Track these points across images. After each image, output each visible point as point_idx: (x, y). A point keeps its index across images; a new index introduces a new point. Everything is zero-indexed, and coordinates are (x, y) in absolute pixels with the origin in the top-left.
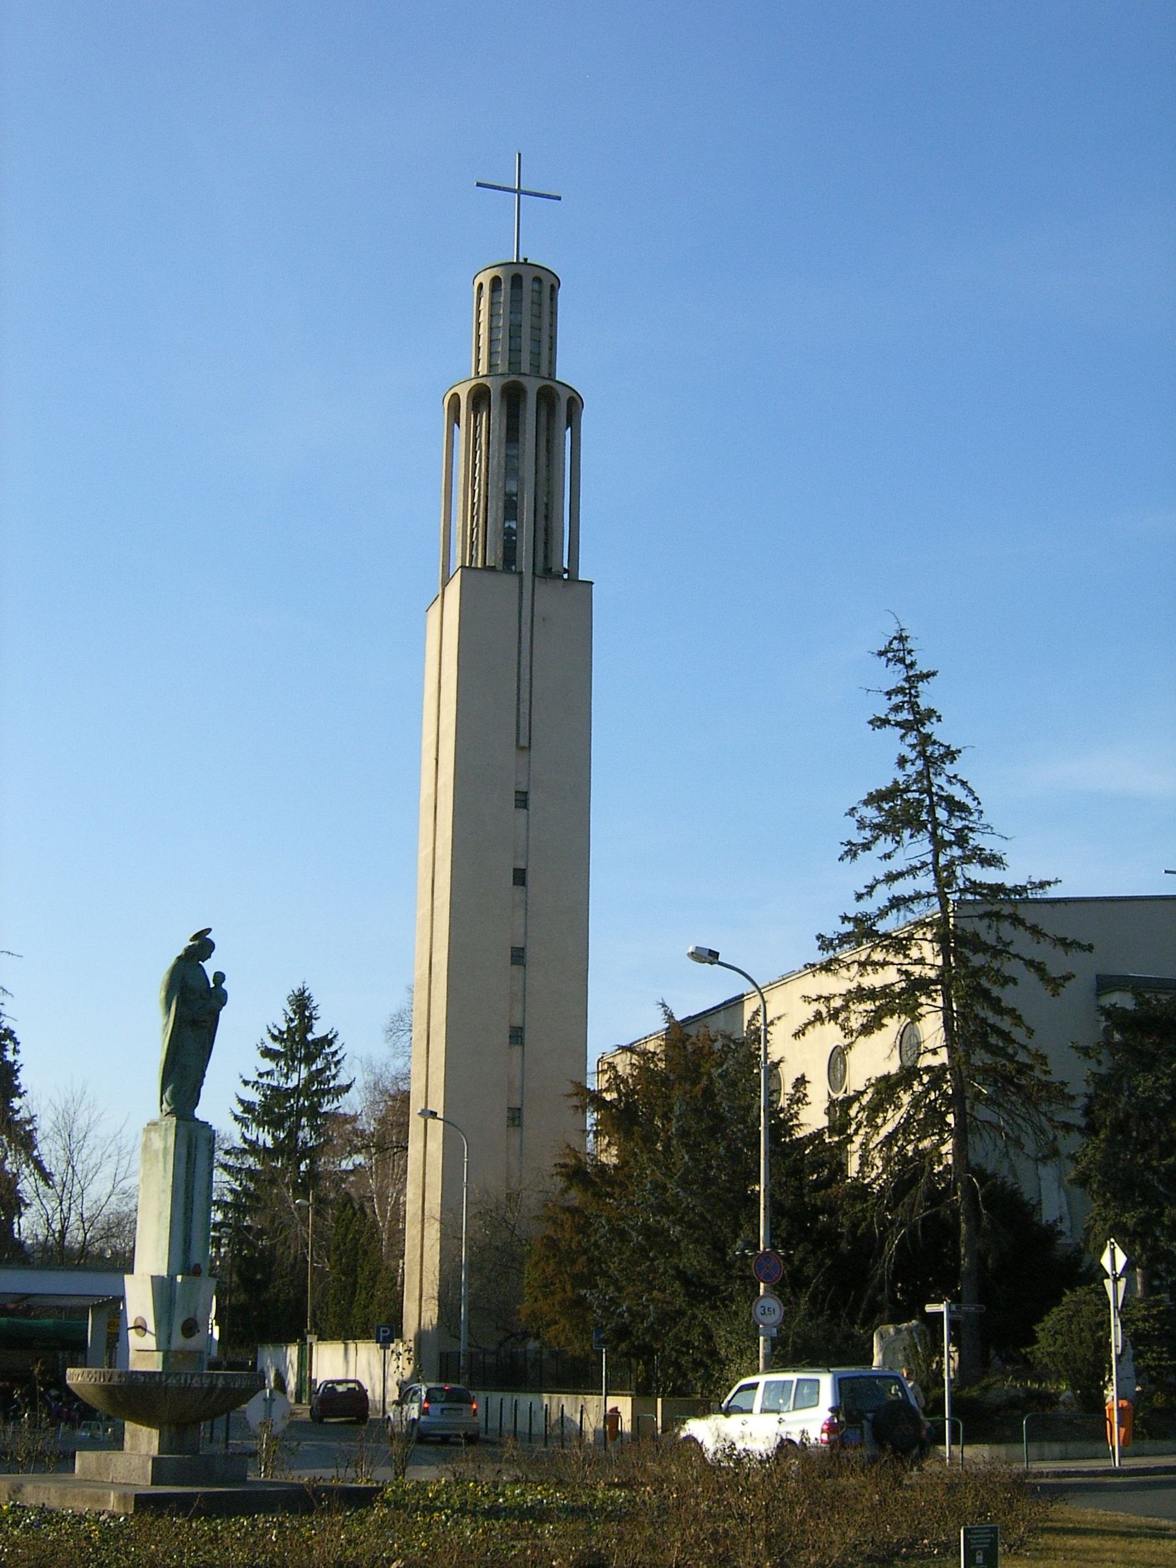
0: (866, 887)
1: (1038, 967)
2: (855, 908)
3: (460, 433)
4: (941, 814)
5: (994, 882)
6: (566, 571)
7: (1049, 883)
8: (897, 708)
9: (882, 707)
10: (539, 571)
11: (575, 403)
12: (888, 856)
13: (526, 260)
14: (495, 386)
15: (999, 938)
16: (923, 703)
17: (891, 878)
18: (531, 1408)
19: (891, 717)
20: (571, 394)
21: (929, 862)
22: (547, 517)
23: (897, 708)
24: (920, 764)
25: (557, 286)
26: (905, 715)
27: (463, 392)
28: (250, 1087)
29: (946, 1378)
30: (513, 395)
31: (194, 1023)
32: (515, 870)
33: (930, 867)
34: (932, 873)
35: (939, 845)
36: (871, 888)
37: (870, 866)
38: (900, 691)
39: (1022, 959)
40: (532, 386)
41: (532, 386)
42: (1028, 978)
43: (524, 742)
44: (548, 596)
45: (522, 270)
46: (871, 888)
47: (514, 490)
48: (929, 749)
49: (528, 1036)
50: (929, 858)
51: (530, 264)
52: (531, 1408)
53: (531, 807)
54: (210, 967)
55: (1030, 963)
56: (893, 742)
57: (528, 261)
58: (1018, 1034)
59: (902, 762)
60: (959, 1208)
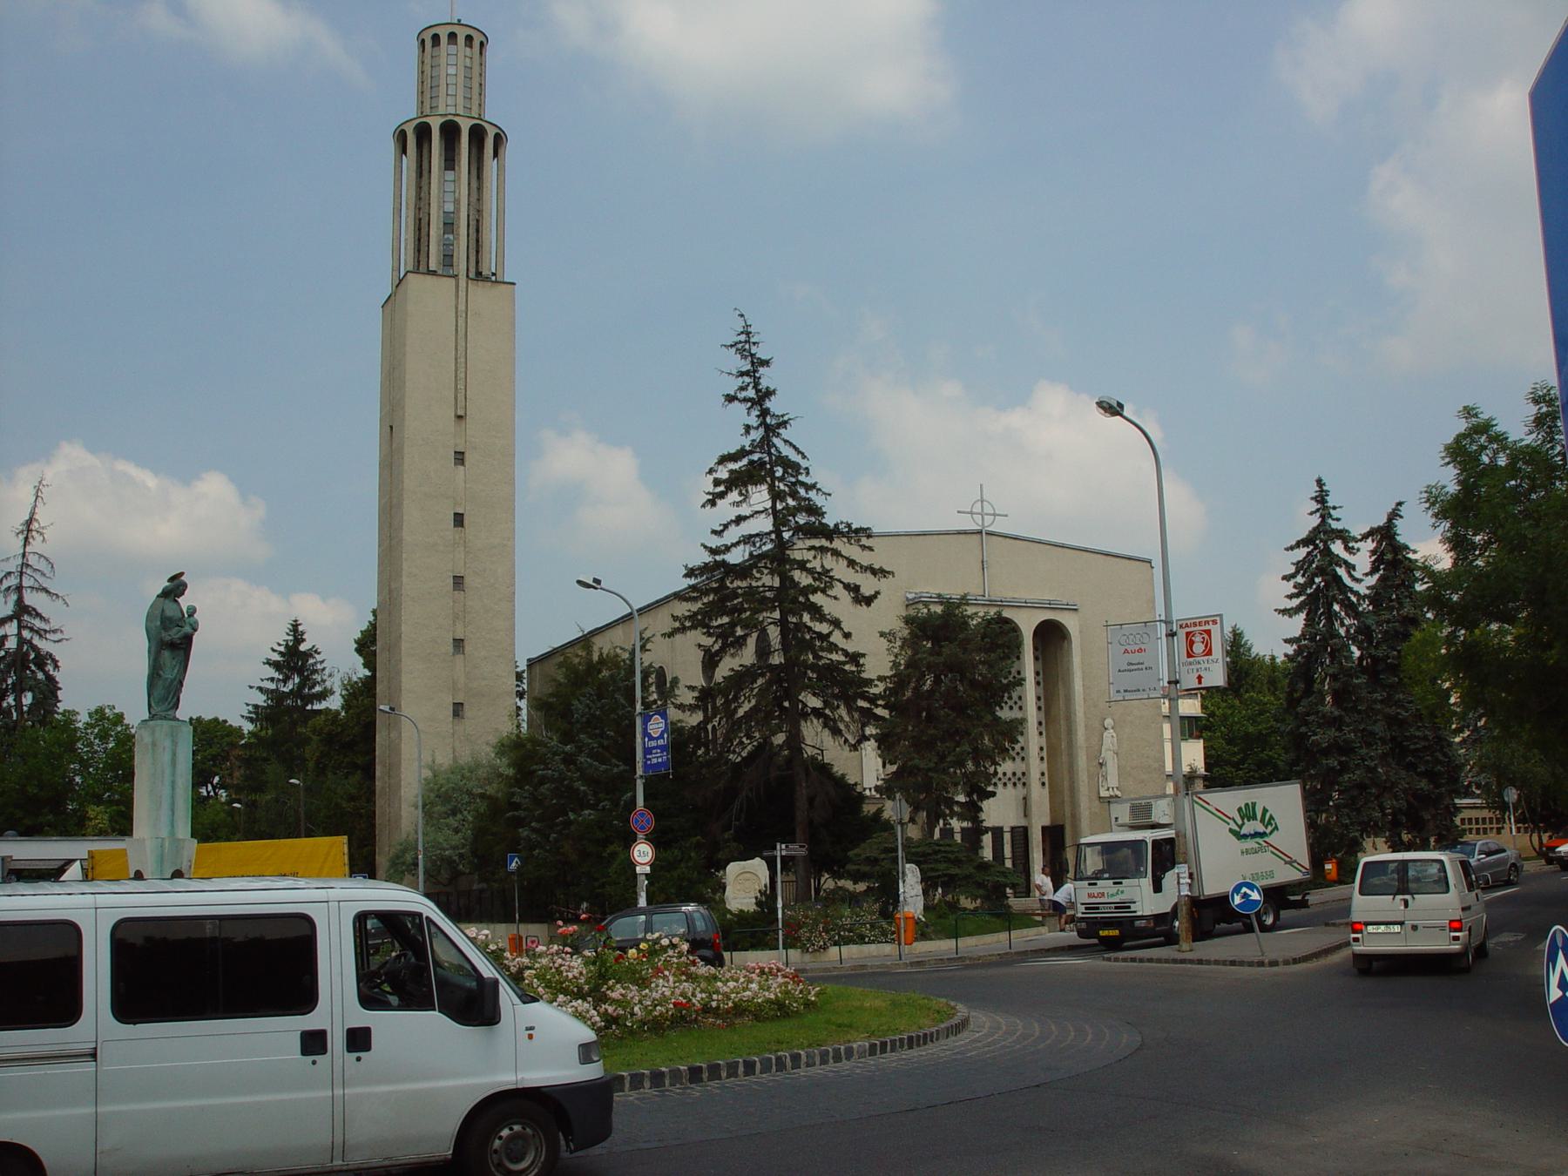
0: (720, 525)
1: (853, 589)
2: (715, 542)
4: (779, 472)
5: (1307, 533)
6: (494, 274)
7: (29, 522)
8: (742, 389)
9: (732, 385)
10: (472, 275)
12: (737, 504)
13: (459, 21)
14: (435, 124)
15: (822, 566)
16: (764, 384)
17: (739, 520)
18: (333, 1142)
19: (739, 395)
21: (768, 507)
22: (478, 231)
23: (742, 389)
24: (761, 430)
25: (485, 43)
26: (751, 393)
28: (254, 689)
29: (780, 916)
31: (172, 646)
32: (455, 514)
33: (770, 511)
34: (771, 516)
35: (776, 496)
36: (726, 526)
37: (727, 508)
38: (747, 373)
39: (841, 582)
40: (465, 126)
41: (465, 126)
42: (846, 597)
43: (460, 412)
44: (480, 295)
45: (456, 29)
46: (726, 526)
47: (452, 209)
48: (768, 420)
49: (468, 648)
50: (769, 504)
51: (463, 25)
52: (333, 1142)
53: (467, 463)
54: (184, 602)
55: (847, 587)
56: (741, 415)
57: (462, 22)
58: (836, 638)
59: (748, 428)
60: (752, 577)
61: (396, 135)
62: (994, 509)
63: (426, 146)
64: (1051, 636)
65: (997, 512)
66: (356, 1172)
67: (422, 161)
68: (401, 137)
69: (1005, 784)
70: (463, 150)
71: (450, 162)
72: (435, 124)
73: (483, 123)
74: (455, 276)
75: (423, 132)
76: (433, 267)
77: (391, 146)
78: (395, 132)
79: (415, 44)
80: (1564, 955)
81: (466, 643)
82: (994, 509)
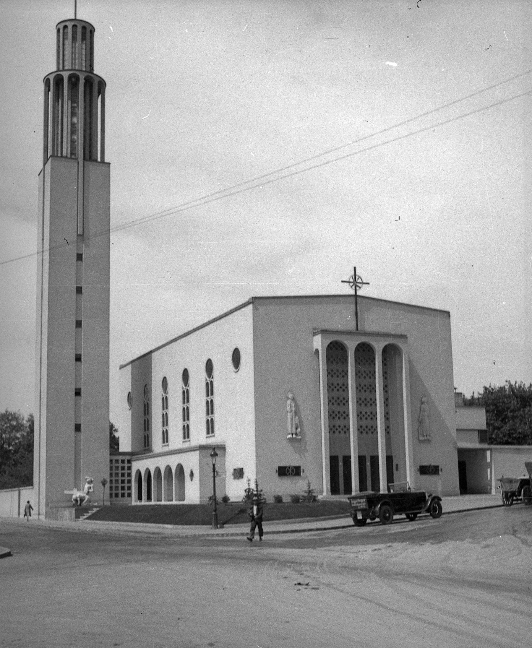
3: (51, 94)
11: (102, 84)
14: (66, 75)
18: (7, 262)
20: (98, 79)
27: (51, 78)
30: (74, 80)
45: (76, 23)
52: (7, 262)
61: (45, 80)
62: (362, 280)
63: (61, 87)
64: (214, 436)
65: (364, 281)
66: (50, 153)
67: (59, 49)
68: (47, 81)
69: (365, 391)
70: (80, 88)
71: (74, 99)
72: (66, 75)
73: (93, 76)
74: (77, 159)
75: (59, 80)
76: (64, 154)
77: (42, 87)
78: (44, 78)
79: (55, 31)
80: (259, 527)
81: (111, 165)
82: (362, 280)
